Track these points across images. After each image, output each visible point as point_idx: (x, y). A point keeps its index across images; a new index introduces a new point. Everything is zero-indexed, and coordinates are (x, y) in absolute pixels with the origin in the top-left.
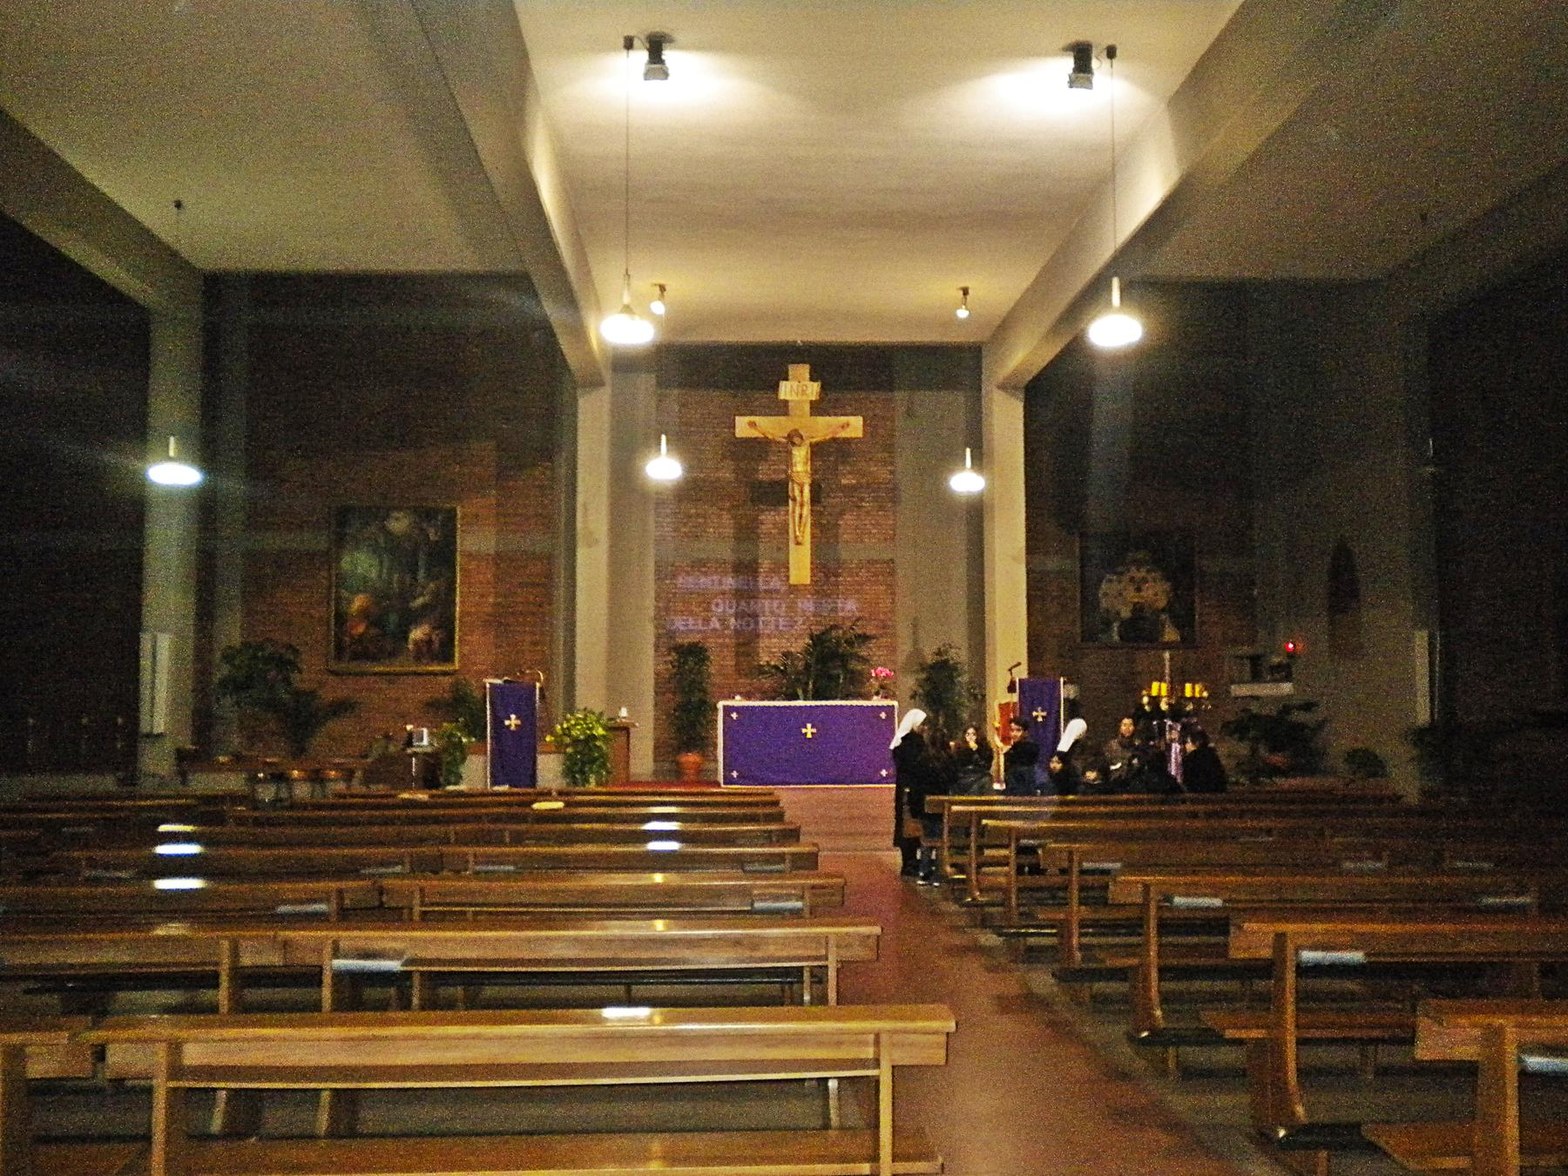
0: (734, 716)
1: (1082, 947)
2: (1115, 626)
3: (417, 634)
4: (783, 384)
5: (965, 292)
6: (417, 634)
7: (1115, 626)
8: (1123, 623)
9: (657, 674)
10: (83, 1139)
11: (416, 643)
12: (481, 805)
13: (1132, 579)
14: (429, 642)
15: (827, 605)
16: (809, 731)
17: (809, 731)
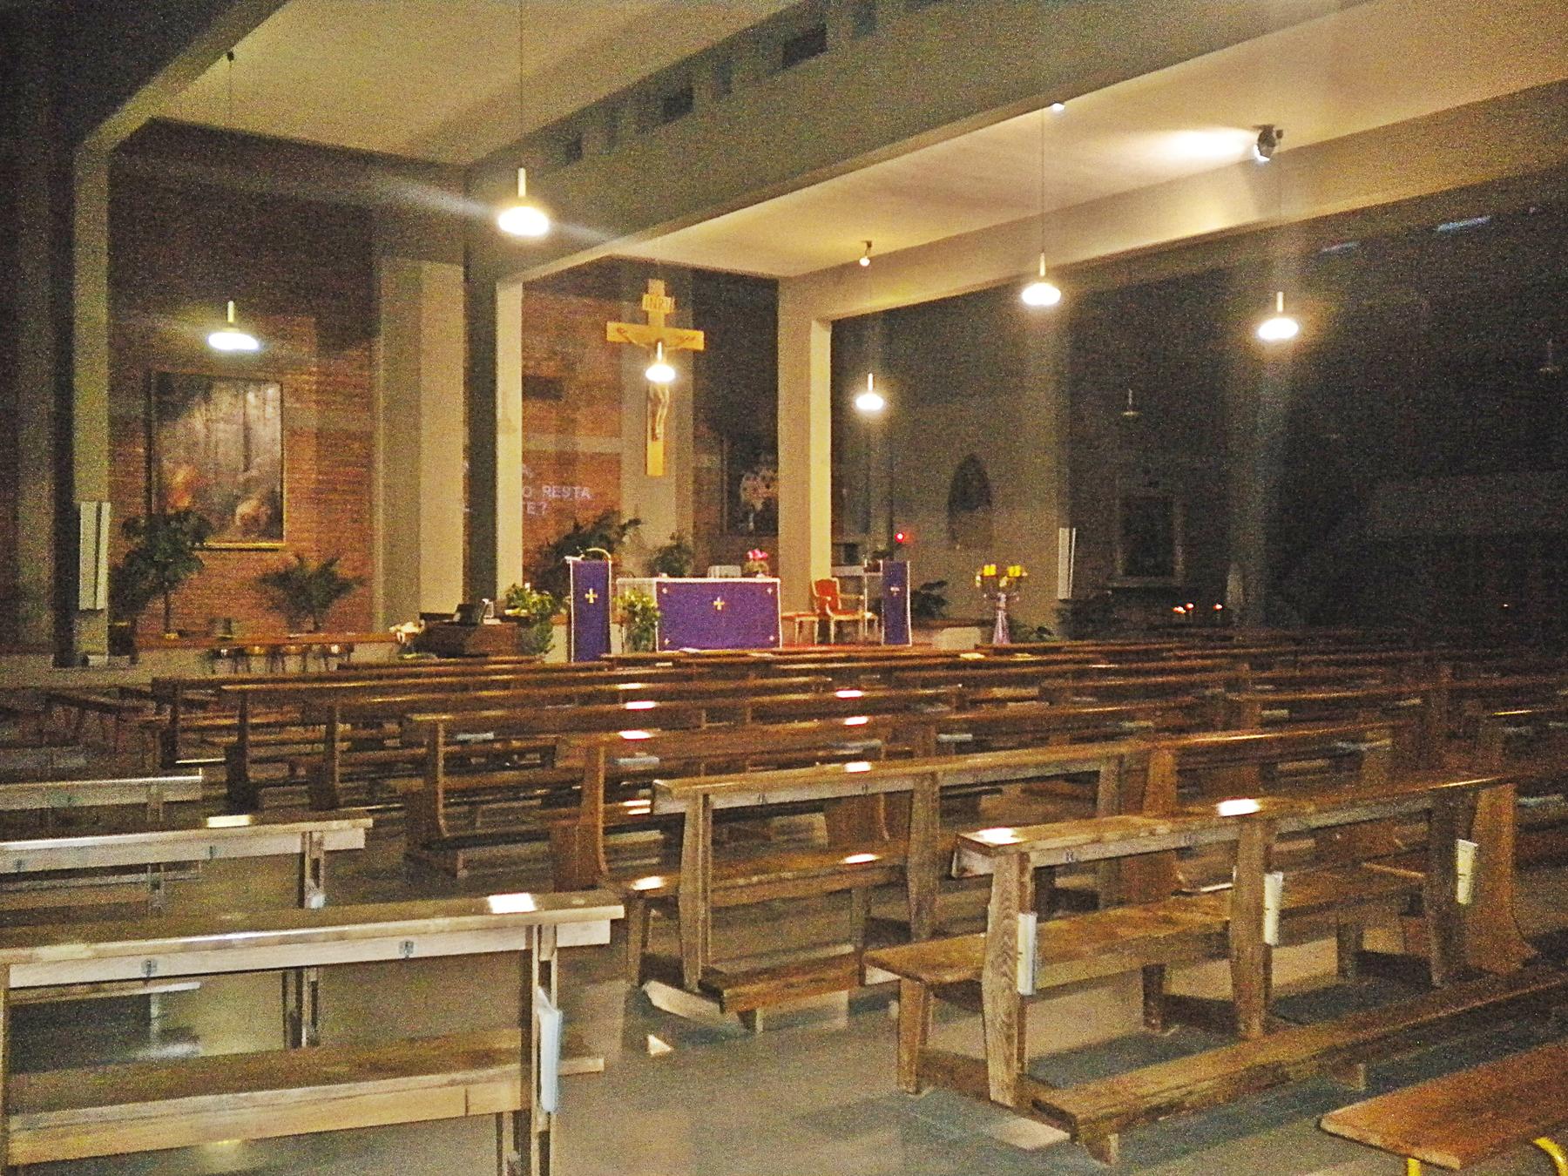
0: (665, 591)
1: (447, 816)
2: (752, 516)
3: (244, 509)
4: (645, 297)
5: (869, 245)
6: (244, 509)
7: (752, 516)
8: (756, 515)
9: (526, 552)
10: (500, 1142)
11: (242, 517)
12: (576, 681)
13: (764, 478)
14: (256, 519)
15: (567, 491)
16: (719, 604)
17: (719, 604)
